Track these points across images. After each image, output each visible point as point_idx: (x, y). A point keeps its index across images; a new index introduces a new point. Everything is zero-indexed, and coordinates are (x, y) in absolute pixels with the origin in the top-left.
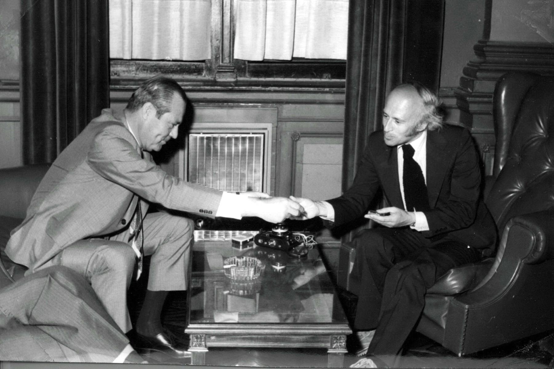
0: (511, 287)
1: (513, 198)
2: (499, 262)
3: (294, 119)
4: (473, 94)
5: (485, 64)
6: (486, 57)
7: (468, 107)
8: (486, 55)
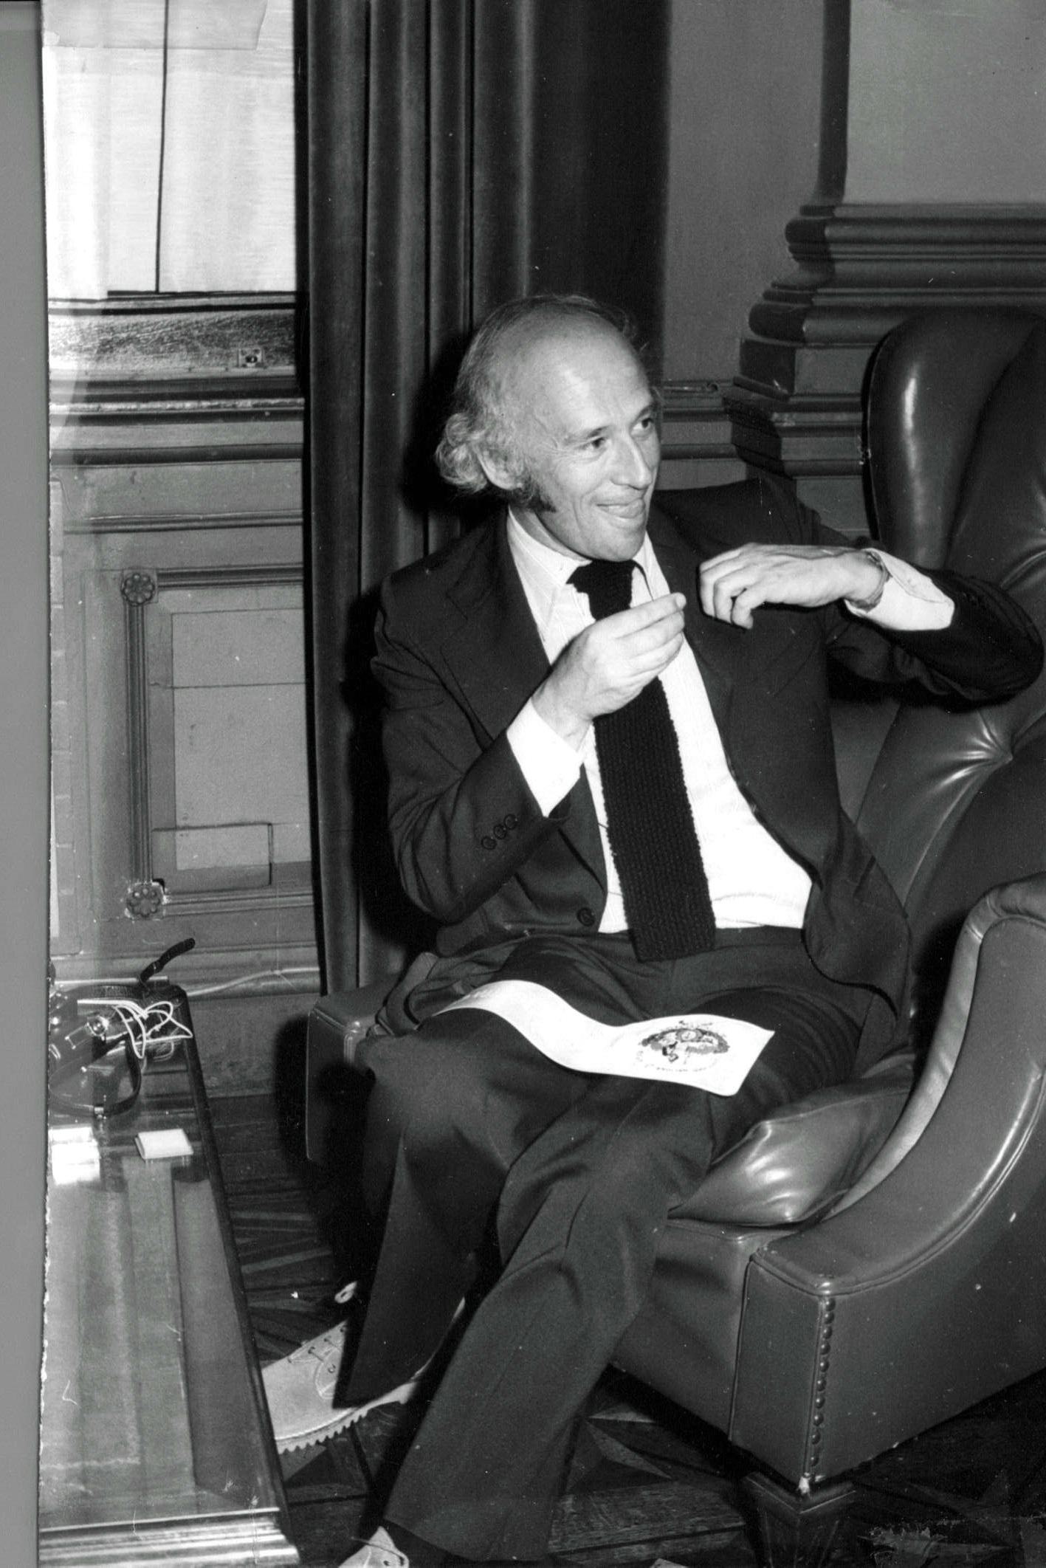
0: (1001, 1181)
1: (968, 785)
2: (943, 1071)
3: (152, 523)
4: (793, 400)
5: (829, 290)
6: (832, 261)
7: (778, 447)
8: (835, 256)
